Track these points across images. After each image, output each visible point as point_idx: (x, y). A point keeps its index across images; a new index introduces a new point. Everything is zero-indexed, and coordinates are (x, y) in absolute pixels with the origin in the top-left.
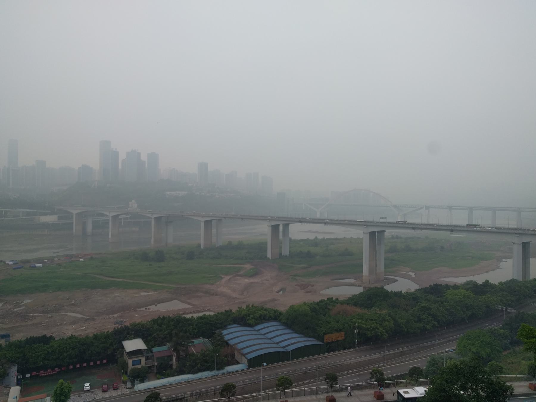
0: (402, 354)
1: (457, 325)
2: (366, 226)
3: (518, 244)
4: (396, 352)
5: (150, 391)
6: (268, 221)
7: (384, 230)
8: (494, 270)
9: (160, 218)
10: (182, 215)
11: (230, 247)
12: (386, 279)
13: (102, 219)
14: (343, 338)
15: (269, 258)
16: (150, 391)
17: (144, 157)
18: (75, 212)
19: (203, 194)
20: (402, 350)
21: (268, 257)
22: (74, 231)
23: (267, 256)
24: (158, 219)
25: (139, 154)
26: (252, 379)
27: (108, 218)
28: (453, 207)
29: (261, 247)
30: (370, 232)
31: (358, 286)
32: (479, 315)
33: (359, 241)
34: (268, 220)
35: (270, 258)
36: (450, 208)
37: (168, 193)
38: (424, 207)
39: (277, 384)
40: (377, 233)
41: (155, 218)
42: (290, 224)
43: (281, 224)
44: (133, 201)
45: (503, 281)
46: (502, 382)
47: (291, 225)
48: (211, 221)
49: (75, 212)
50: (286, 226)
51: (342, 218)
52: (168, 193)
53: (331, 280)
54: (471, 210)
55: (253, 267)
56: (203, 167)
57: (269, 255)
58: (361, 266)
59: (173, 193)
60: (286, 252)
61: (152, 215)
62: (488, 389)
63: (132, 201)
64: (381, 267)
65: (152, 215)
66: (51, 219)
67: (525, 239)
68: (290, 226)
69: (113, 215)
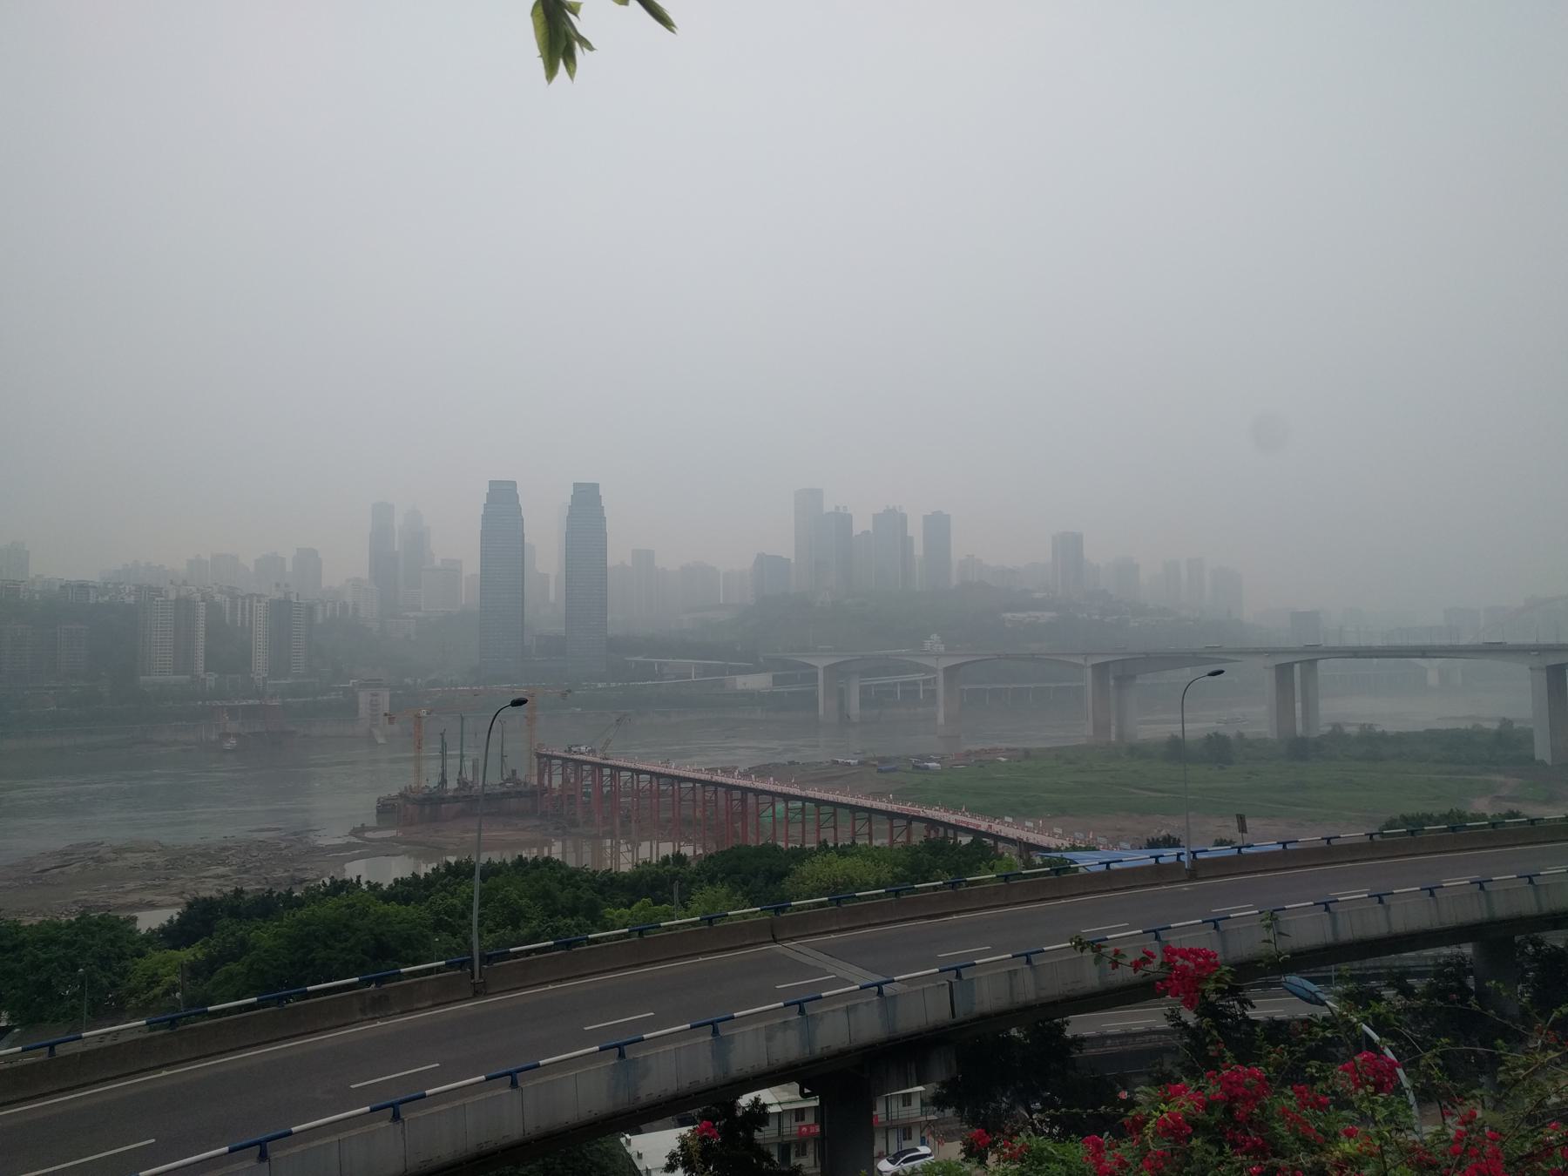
2: (1536, 653)
5: (192, 1015)
7: (816, 664)
9: (1106, 664)
11: (1337, 735)
13: (900, 680)
16: (192, 1015)
18: (821, 663)
21: (1537, 757)
22: (821, 712)
23: (1534, 759)
24: (1101, 670)
34: (1266, 653)
35: (1548, 761)
37: (1009, 615)
41: (1094, 666)
43: (1296, 662)
46: (1325, 1029)
47: (1321, 664)
48: (1291, 665)
49: (821, 663)
51: (1398, 641)
63: (932, 637)
65: (1086, 660)
66: (758, 682)
67: (1553, 660)
69: (827, 664)
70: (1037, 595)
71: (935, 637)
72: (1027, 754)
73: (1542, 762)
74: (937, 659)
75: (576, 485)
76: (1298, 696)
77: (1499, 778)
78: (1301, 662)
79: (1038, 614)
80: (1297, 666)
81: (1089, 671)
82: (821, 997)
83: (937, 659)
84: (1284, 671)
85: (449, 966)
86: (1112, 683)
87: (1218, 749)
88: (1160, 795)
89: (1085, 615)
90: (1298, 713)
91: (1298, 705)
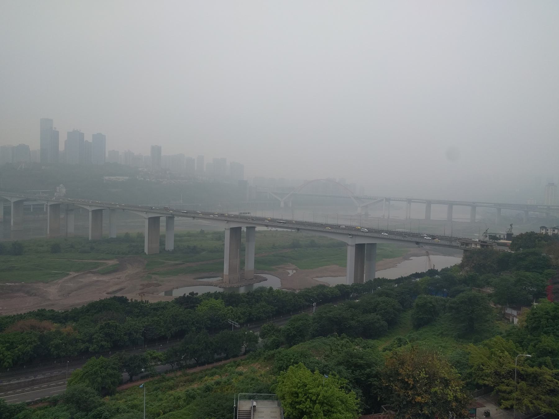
0: (33, 383)
1: (168, 343)
3: (351, 246)
4: (23, 381)
6: (145, 213)
8: (390, 268)
12: (256, 277)
15: (145, 254)
17: (88, 138)
20: (33, 378)
25: (82, 135)
27: (10, 205)
28: (413, 200)
30: (230, 228)
31: (214, 286)
33: (220, 237)
36: (410, 201)
37: (107, 178)
38: (384, 200)
39: (188, 379)
44: (61, 185)
45: (339, 284)
50: (170, 218)
52: (107, 178)
53: (194, 279)
54: (451, 205)
55: (118, 262)
56: (156, 150)
57: (146, 251)
58: (222, 263)
59: (112, 178)
60: (170, 246)
61: (47, 203)
64: (250, 265)
69: (15, 200)
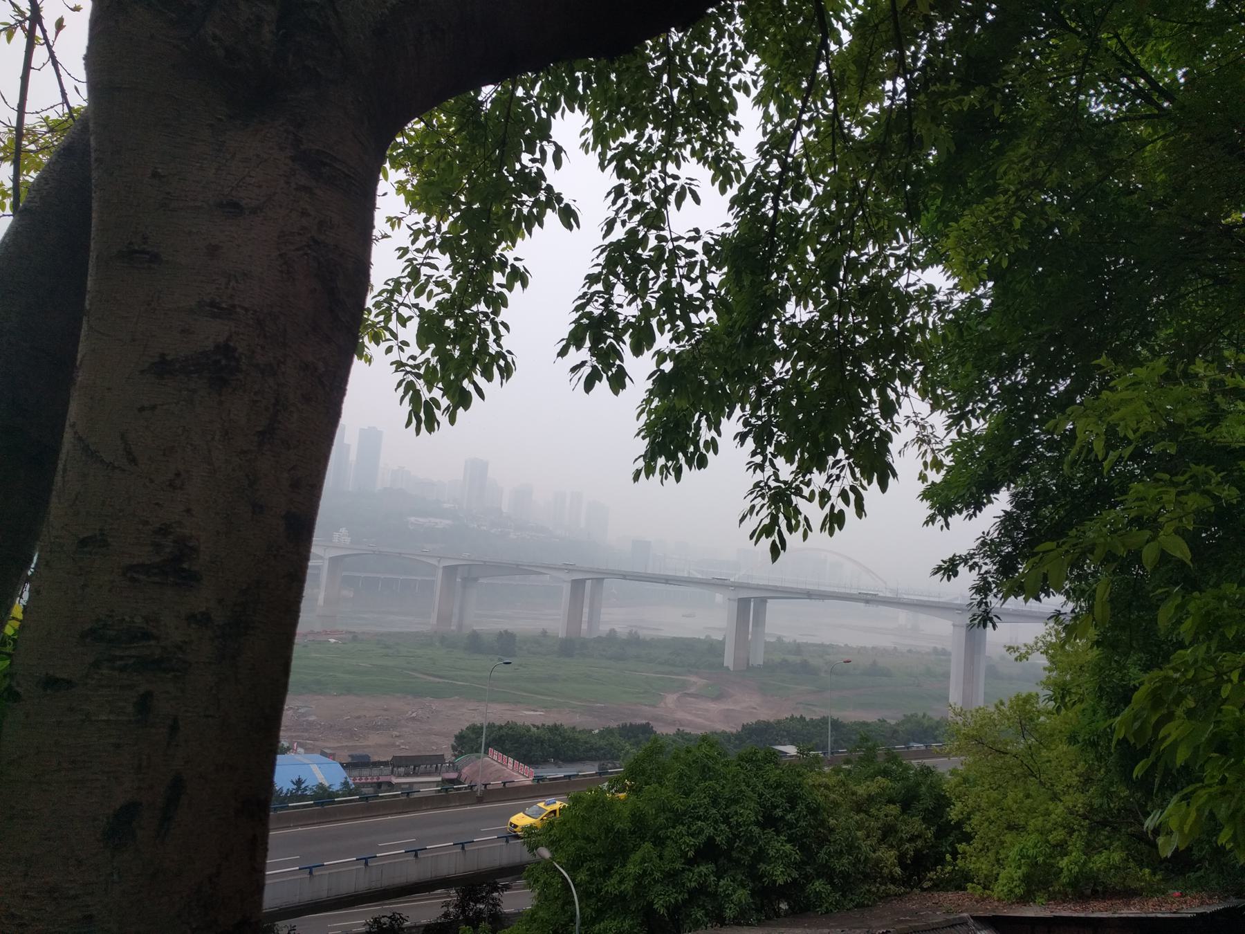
9: (455, 568)
10: (400, 554)
11: (612, 637)
14: (1103, 392)
19: (485, 528)
21: (725, 665)
24: (450, 571)
26: (572, 220)
29: (714, 649)
32: (1172, 164)
37: (412, 519)
40: (752, 604)
42: (769, 600)
43: (589, 579)
47: (771, 604)
48: (584, 581)
52: (412, 519)
59: (422, 520)
61: (439, 561)
62: (1036, 485)
65: (439, 561)
68: (768, 605)
70: (446, 506)
71: (343, 530)
72: (355, 638)
73: (727, 668)
74: (325, 550)
75: (637, 357)
76: (587, 601)
77: (693, 679)
78: (592, 579)
79: (437, 520)
80: (588, 583)
81: (440, 572)
82: (376, 857)
83: (325, 550)
84: (578, 585)
85: (316, 805)
86: (459, 580)
87: (506, 644)
88: (438, 680)
89: (476, 526)
90: (585, 618)
91: (586, 610)
